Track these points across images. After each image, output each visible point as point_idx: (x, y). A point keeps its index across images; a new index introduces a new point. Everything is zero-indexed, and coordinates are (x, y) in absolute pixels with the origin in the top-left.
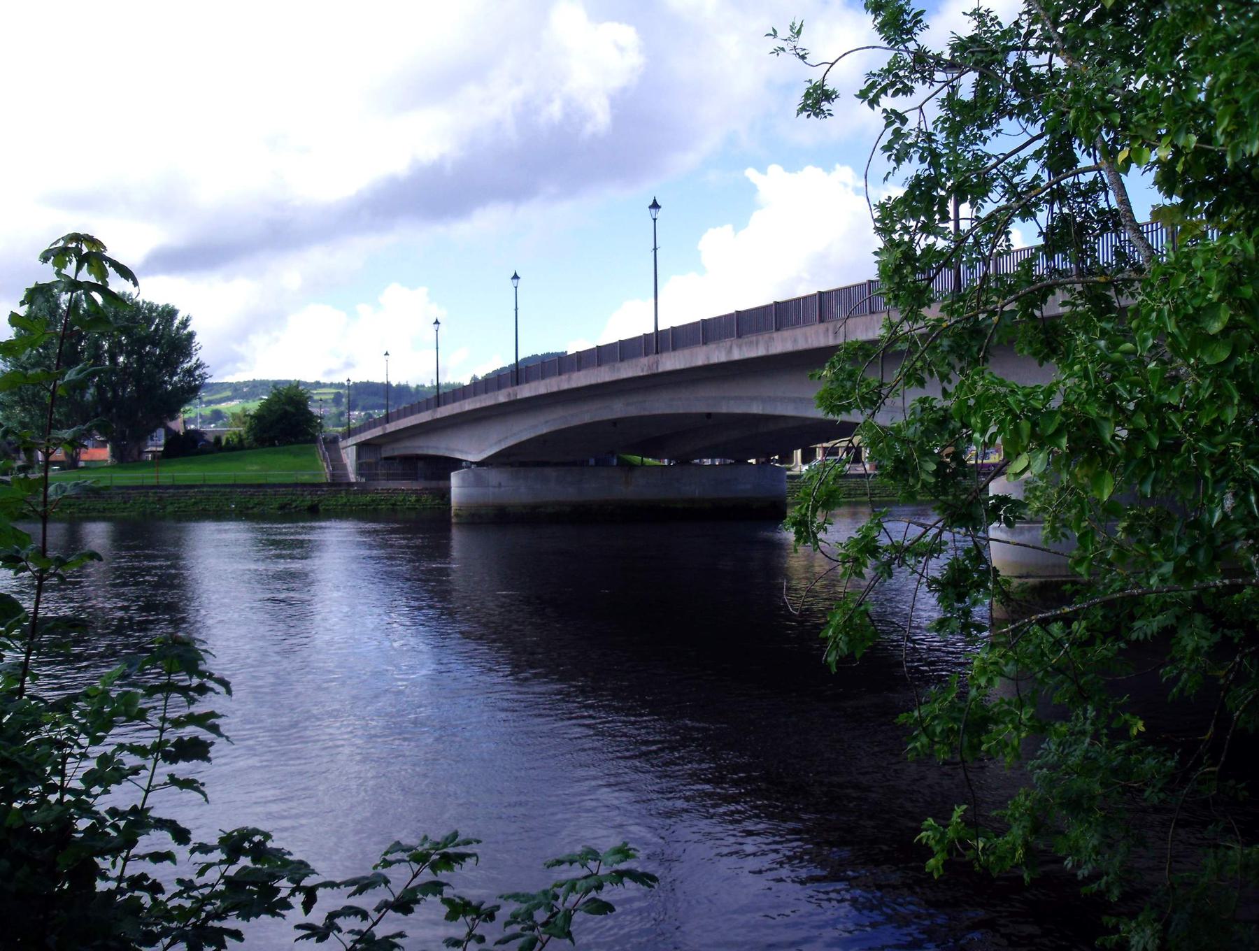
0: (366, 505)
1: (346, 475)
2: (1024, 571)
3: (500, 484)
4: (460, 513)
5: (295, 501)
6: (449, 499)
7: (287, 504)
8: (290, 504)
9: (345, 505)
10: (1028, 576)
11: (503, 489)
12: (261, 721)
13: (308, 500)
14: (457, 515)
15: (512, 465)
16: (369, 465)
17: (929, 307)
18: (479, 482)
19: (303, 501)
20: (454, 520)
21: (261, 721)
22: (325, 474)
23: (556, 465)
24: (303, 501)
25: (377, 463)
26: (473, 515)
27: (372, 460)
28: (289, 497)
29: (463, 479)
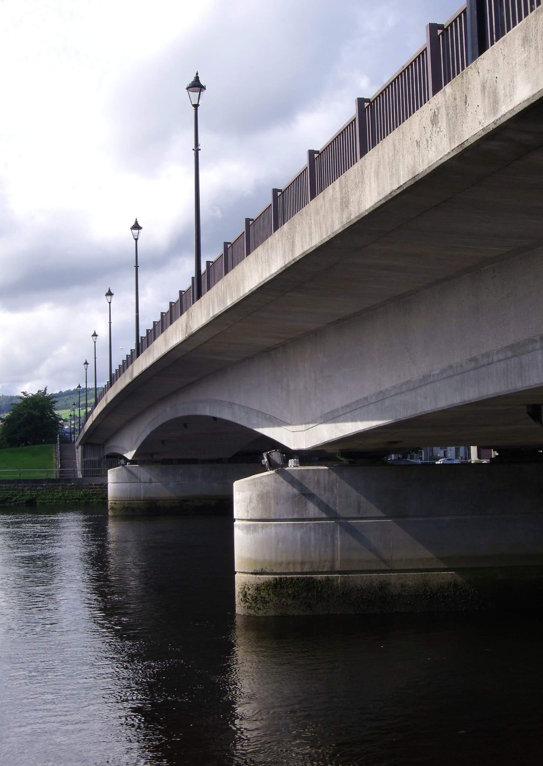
0: (79, 499)
1: (75, 472)
2: (259, 569)
3: (151, 480)
4: (115, 506)
5: (16, 495)
6: (107, 495)
7: (7, 498)
8: (11, 499)
9: (60, 498)
10: (262, 573)
11: (153, 484)
12: (62, 628)
13: (28, 494)
14: (112, 508)
15: (156, 462)
16: (93, 463)
17: (200, 150)
18: (133, 477)
19: (22, 496)
20: (110, 513)
21: (62, 628)
22: (54, 472)
23: (204, 462)
24: (22, 496)
25: (100, 461)
26: (125, 509)
27: (97, 458)
28: (11, 492)
29: (117, 476)
